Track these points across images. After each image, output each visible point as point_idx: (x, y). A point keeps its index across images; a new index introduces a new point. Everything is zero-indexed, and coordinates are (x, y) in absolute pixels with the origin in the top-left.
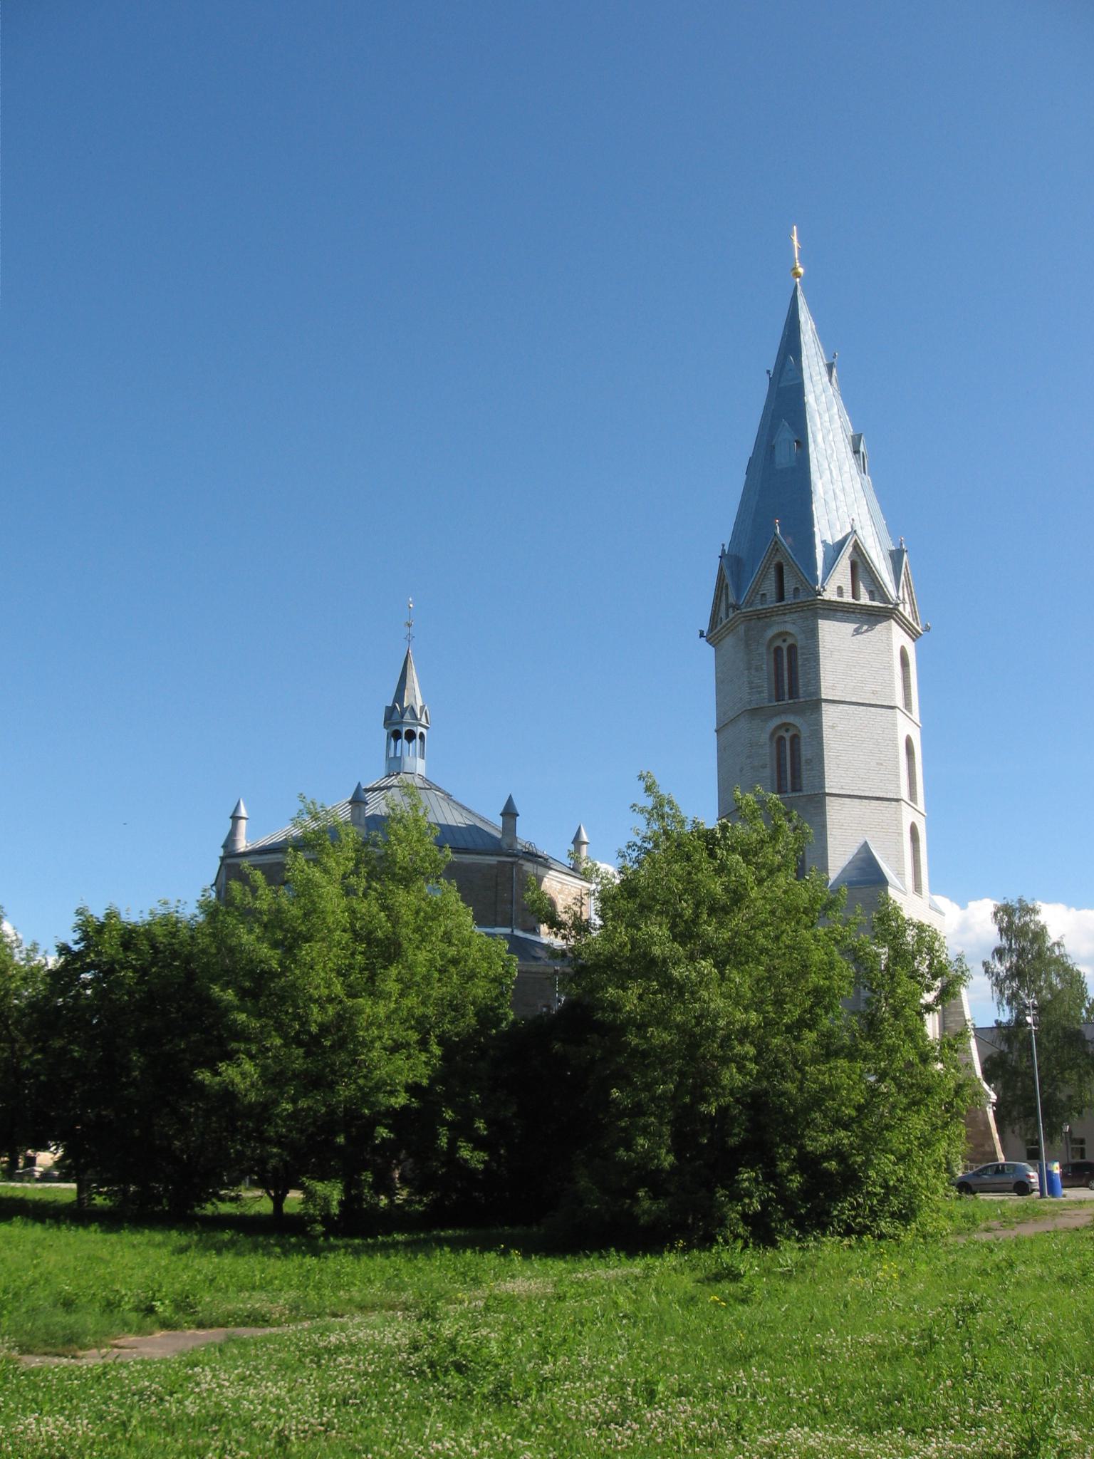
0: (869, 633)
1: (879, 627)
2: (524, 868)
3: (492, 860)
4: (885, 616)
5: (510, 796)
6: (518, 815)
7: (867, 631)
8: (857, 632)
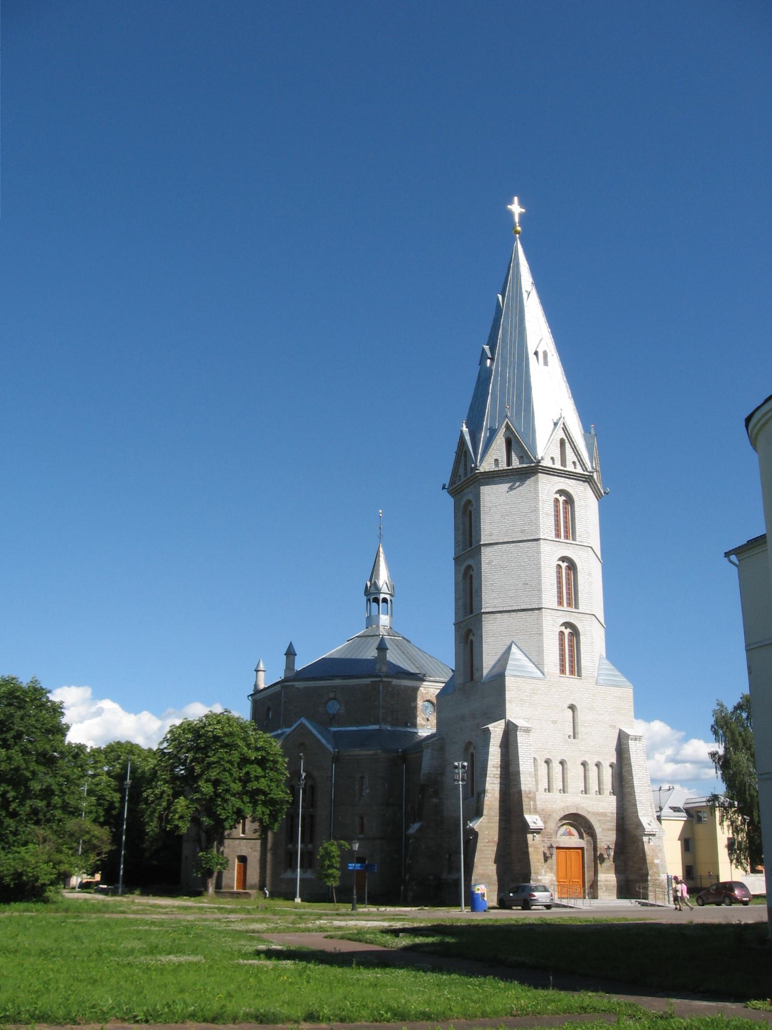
0: (521, 488)
1: (528, 482)
2: (393, 683)
3: (368, 681)
4: (533, 473)
5: (291, 643)
6: (387, 649)
7: (519, 486)
8: (511, 489)
